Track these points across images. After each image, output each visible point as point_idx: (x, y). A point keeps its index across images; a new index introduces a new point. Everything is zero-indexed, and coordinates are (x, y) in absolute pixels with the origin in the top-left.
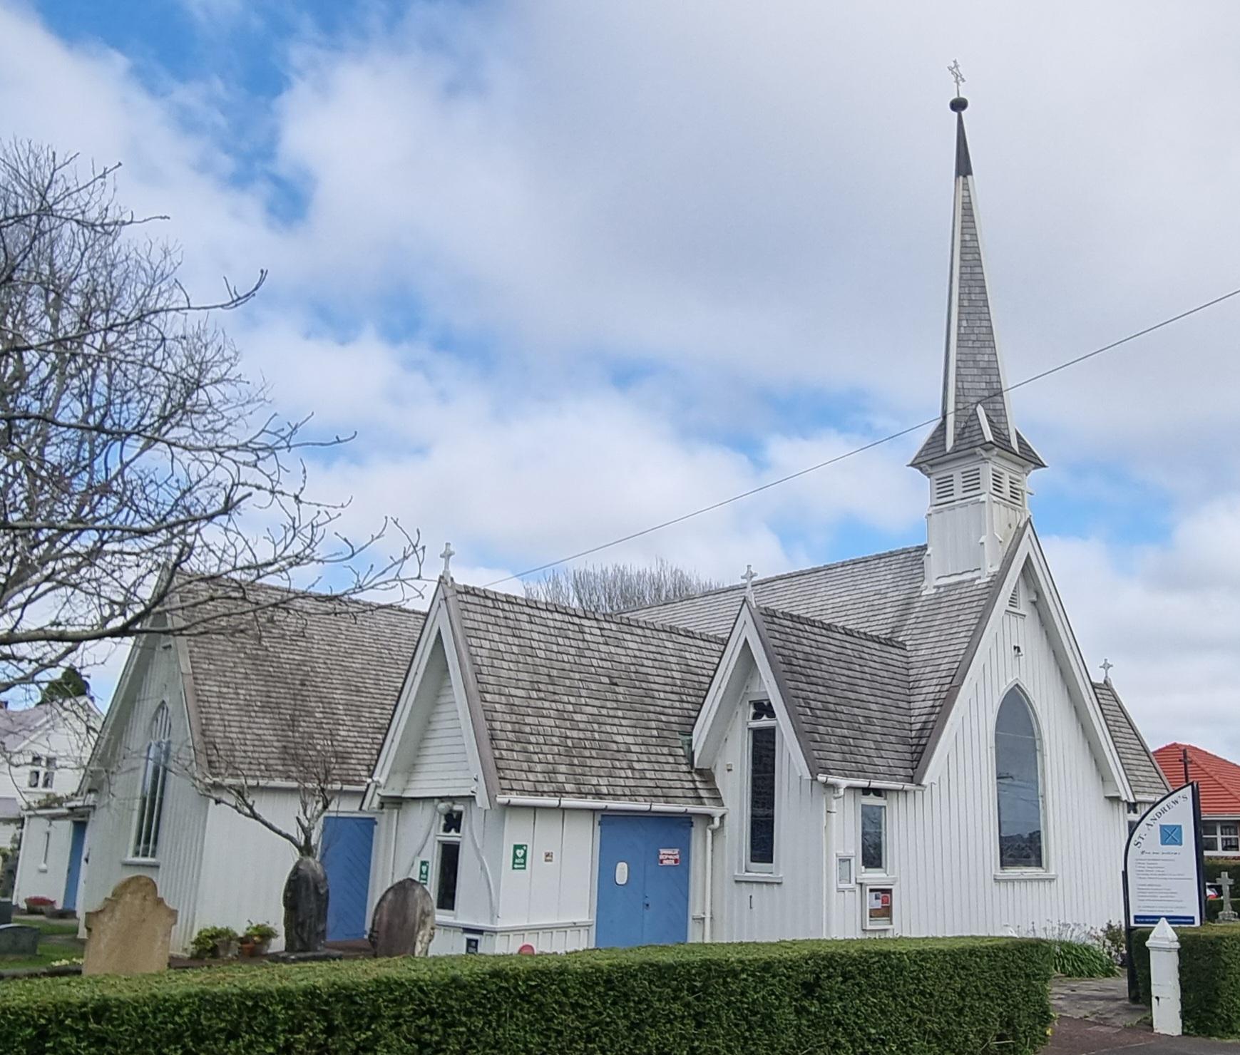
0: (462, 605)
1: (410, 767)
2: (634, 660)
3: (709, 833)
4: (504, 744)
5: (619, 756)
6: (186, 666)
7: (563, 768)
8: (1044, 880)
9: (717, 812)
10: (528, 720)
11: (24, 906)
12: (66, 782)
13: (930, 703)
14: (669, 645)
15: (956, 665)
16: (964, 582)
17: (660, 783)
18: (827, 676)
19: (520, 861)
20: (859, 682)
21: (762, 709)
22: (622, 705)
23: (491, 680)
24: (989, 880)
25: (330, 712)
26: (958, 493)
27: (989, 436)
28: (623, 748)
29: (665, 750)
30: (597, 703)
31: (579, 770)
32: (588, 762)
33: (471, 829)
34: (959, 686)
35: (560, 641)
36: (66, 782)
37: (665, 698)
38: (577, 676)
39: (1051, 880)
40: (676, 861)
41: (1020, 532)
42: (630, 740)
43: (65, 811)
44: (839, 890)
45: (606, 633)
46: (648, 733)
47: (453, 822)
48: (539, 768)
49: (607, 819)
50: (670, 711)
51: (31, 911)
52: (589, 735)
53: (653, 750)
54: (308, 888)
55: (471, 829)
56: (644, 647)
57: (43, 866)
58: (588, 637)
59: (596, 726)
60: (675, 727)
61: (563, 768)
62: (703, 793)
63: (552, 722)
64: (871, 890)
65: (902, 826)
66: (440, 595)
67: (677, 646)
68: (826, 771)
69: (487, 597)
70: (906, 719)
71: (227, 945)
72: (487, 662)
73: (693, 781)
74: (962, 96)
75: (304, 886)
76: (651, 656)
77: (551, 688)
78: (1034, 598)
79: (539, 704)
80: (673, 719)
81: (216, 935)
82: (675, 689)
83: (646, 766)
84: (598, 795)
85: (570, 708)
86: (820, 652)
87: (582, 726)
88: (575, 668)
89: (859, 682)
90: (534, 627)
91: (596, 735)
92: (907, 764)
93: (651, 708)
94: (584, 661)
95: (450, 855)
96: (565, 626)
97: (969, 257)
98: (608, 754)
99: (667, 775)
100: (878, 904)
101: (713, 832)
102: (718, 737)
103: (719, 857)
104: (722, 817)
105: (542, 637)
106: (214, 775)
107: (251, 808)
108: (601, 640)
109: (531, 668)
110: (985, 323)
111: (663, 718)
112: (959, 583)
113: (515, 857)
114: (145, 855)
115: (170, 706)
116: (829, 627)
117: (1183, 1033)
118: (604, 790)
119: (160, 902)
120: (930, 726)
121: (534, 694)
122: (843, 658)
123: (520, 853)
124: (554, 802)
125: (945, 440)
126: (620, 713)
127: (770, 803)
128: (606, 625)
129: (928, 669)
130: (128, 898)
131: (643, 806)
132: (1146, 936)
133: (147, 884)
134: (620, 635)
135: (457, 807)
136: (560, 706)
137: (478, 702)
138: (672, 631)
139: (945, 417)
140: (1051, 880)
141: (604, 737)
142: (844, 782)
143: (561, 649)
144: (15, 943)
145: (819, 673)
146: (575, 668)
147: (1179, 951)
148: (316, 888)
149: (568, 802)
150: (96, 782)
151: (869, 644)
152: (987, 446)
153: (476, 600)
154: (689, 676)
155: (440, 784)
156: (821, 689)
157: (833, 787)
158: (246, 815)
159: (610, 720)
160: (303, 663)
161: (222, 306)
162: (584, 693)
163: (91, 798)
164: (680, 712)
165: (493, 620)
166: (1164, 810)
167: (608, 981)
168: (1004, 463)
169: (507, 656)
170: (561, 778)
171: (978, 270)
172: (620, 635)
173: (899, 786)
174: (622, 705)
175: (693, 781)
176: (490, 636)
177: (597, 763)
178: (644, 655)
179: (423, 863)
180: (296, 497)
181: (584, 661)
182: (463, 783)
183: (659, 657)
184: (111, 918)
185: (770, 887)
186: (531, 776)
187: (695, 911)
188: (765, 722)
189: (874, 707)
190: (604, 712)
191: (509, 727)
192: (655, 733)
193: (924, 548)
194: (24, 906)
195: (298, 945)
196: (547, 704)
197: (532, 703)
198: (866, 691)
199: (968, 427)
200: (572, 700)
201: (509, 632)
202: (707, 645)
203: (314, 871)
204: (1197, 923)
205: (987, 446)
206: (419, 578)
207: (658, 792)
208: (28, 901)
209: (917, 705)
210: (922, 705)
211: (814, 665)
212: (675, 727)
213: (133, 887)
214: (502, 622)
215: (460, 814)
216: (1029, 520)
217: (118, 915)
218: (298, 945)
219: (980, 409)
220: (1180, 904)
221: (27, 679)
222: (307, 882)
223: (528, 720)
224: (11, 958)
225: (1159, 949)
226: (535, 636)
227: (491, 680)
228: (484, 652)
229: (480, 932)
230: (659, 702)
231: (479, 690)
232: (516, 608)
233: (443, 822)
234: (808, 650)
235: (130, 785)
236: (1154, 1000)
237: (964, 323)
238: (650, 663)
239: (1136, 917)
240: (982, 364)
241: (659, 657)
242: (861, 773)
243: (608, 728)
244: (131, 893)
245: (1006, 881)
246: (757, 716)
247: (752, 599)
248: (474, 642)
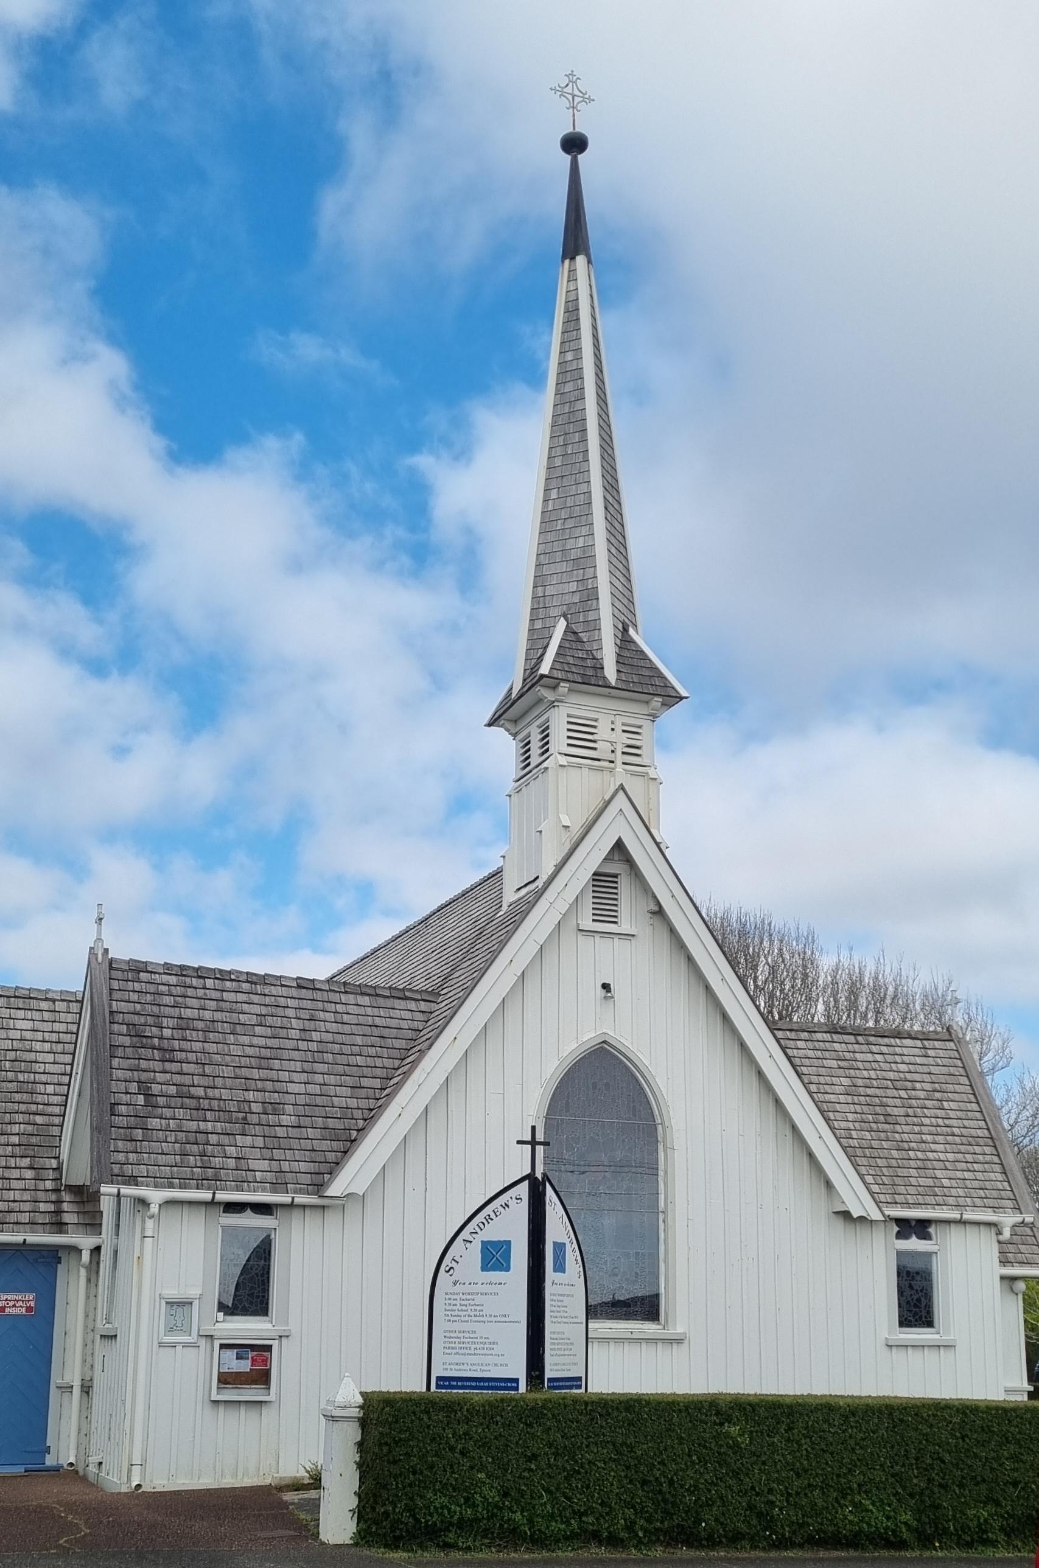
40: (29, 1309)
64: (222, 1346)
65: (304, 1256)
74: (577, 130)
124: (955, 1215)
142: (156, 1196)
157: (143, 1203)
187: (55, 1380)
204: (523, 1388)
220: (499, 1360)
239: (439, 1379)
240: (573, 555)
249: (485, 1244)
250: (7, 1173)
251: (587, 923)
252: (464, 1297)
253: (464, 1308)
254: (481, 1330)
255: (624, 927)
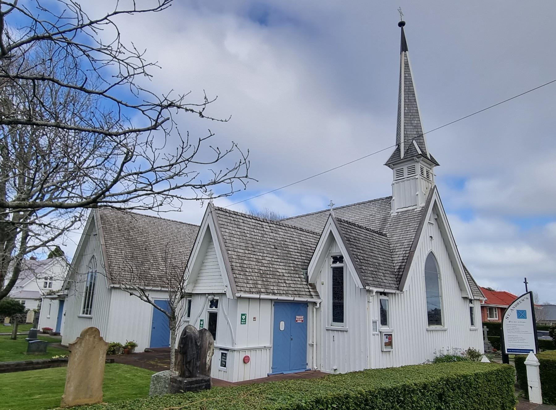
0: (217, 215)
1: (196, 282)
2: (283, 239)
3: (315, 309)
4: (237, 272)
5: (280, 278)
6: (102, 242)
7: (260, 282)
8: (443, 330)
9: (318, 301)
10: (246, 262)
11: (42, 331)
12: (57, 286)
13: (402, 258)
14: (295, 234)
15: (411, 243)
16: (409, 210)
17: (296, 289)
18: (362, 246)
19: (243, 321)
20: (374, 249)
21: (339, 259)
22: (280, 257)
23: (230, 245)
24: (425, 330)
25: (156, 260)
26: (406, 175)
27: (420, 152)
28: (281, 274)
29: (297, 276)
30: (271, 256)
31: (266, 283)
32: (269, 280)
33: (222, 305)
34: (414, 251)
35: (255, 230)
36: (57, 286)
37: (295, 254)
38: (262, 245)
39: (445, 330)
41: (432, 191)
42: (284, 271)
43: (57, 296)
44: (374, 335)
45: (271, 228)
46: (290, 268)
47: (214, 303)
48: (251, 282)
49: (277, 303)
50: (297, 260)
51: (44, 333)
52: (268, 269)
53: (292, 275)
54: (192, 342)
55: (222, 305)
56: (286, 234)
57: (49, 316)
58: (265, 229)
59: (271, 265)
60: (300, 266)
61: (260, 282)
62: (313, 293)
63: (254, 263)
66: (209, 210)
67: (298, 234)
68: (368, 285)
69: (226, 212)
70: (392, 264)
71: (119, 350)
72: (228, 238)
73: (308, 288)
75: (190, 341)
76: (289, 238)
77: (253, 249)
78: (437, 217)
79: (249, 255)
80: (299, 263)
81: (115, 345)
82: (299, 251)
83: (291, 282)
84: (274, 294)
85: (261, 258)
86: (359, 237)
87: (265, 265)
88: (261, 241)
89: (374, 249)
90: (245, 225)
91: (271, 269)
92: (395, 283)
93: (291, 259)
94: (265, 239)
95: (213, 318)
96: (256, 225)
97: (408, 83)
98: (276, 277)
99: (299, 286)
100: (387, 340)
101: (316, 309)
102: (318, 271)
103: (320, 318)
104: (320, 303)
105: (248, 229)
106: (113, 283)
107: (147, 298)
108: (270, 231)
109: (245, 241)
110: (415, 108)
111: (295, 263)
112: (407, 211)
113: (242, 319)
114: (87, 314)
115: (96, 257)
116: (360, 227)
117: (543, 403)
118: (276, 292)
119: (101, 339)
120: (403, 267)
121: (247, 252)
122: (367, 239)
123: (244, 317)
124: (257, 296)
125: (400, 154)
126: (279, 260)
127: (341, 298)
128: (271, 225)
129: (398, 245)
130: (87, 337)
131: (290, 298)
132: (524, 359)
133: (95, 331)
134: (277, 229)
135: (216, 298)
136: (257, 257)
137: (226, 255)
138: (295, 228)
139: (398, 145)
140: (445, 330)
141: (274, 270)
142: (375, 290)
143: (256, 234)
144: (38, 348)
145: (360, 245)
146: (261, 241)
147: (540, 366)
148: (196, 342)
149: (263, 296)
150: (68, 286)
151: (375, 234)
152: (419, 156)
153: (222, 213)
154: (303, 246)
155: (209, 288)
156: (362, 251)
157: (369, 291)
158: (145, 301)
159: (275, 263)
160: (146, 242)
161: (153, 10)
162: (265, 252)
163: (66, 292)
164: (301, 260)
165: (229, 221)
166: (518, 304)
167: (366, 400)
168: (424, 163)
169: (235, 236)
170: (259, 286)
171: (411, 88)
172: (277, 229)
173: (394, 291)
174: (280, 257)
175: (308, 288)
176: (229, 228)
177: (272, 280)
178: (286, 237)
179: (201, 320)
180: (200, 114)
181: (265, 239)
182: (220, 288)
183: (291, 238)
184: (80, 347)
185: (342, 333)
186: (248, 286)
187: (310, 341)
188: (338, 265)
189: (380, 259)
190: (273, 260)
191: (238, 265)
192: (293, 268)
193: (391, 197)
194: (42, 331)
195: (187, 374)
196: (252, 256)
197: (246, 255)
198: (377, 253)
199: (410, 149)
200: (261, 254)
201: (236, 226)
202: (308, 234)
203: (194, 333)
205: (419, 156)
206: (246, 177)
207: (296, 292)
208: (44, 329)
209: (396, 259)
210: (398, 259)
211: (358, 242)
212: (300, 266)
213: (90, 332)
214: (233, 222)
215: (217, 301)
216: (435, 186)
217: (83, 345)
218: (187, 374)
219: (414, 142)
221: (44, 244)
222: (192, 339)
223: (246, 262)
224: (37, 353)
225: (531, 365)
226: (246, 228)
227: (230, 245)
228: (227, 234)
229: (227, 350)
230: (293, 256)
231: (226, 249)
232: (238, 217)
233: (210, 304)
234: (354, 235)
235: (82, 288)
236: (529, 388)
237: (407, 108)
238: (288, 240)
239: (508, 349)
240: (414, 125)
241: (291, 238)
242: (379, 286)
243: (275, 266)
244: (89, 335)
245: (430, 331)
246: (334, 262)
247: (333, 214)
248: (223, 230)
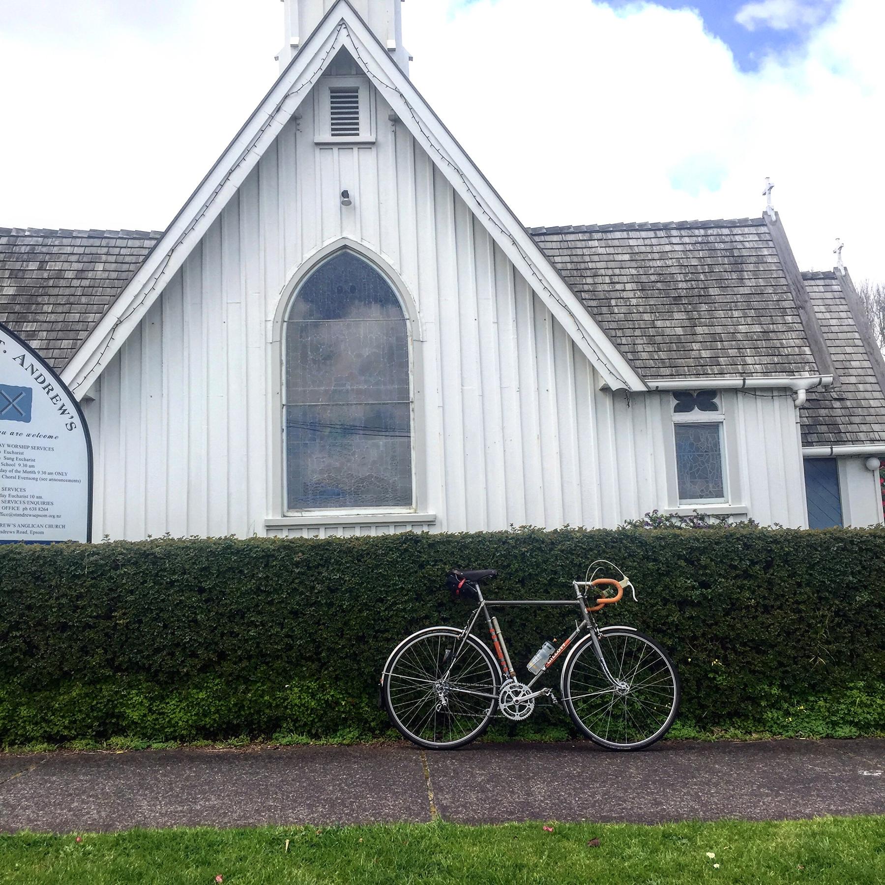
249: (29, 391)
250: (4, 468)
251: (326, 136)
252: (10, 449)
253: (10, 462)
254: (33, 488)
255: (365, 135)
